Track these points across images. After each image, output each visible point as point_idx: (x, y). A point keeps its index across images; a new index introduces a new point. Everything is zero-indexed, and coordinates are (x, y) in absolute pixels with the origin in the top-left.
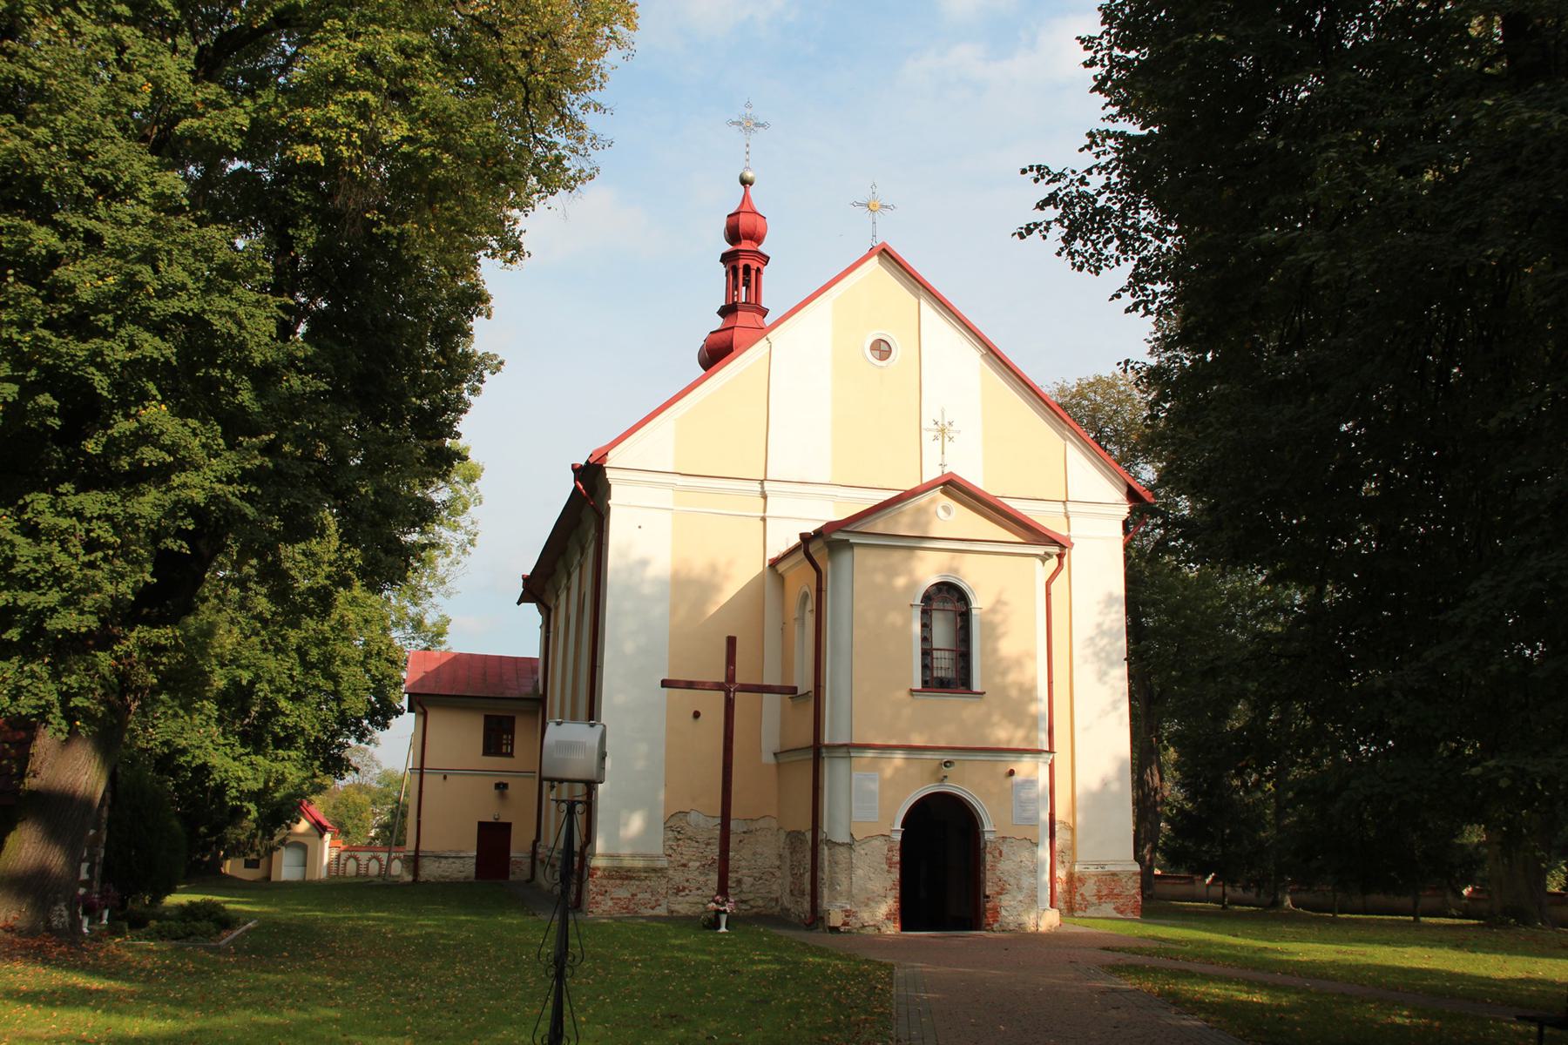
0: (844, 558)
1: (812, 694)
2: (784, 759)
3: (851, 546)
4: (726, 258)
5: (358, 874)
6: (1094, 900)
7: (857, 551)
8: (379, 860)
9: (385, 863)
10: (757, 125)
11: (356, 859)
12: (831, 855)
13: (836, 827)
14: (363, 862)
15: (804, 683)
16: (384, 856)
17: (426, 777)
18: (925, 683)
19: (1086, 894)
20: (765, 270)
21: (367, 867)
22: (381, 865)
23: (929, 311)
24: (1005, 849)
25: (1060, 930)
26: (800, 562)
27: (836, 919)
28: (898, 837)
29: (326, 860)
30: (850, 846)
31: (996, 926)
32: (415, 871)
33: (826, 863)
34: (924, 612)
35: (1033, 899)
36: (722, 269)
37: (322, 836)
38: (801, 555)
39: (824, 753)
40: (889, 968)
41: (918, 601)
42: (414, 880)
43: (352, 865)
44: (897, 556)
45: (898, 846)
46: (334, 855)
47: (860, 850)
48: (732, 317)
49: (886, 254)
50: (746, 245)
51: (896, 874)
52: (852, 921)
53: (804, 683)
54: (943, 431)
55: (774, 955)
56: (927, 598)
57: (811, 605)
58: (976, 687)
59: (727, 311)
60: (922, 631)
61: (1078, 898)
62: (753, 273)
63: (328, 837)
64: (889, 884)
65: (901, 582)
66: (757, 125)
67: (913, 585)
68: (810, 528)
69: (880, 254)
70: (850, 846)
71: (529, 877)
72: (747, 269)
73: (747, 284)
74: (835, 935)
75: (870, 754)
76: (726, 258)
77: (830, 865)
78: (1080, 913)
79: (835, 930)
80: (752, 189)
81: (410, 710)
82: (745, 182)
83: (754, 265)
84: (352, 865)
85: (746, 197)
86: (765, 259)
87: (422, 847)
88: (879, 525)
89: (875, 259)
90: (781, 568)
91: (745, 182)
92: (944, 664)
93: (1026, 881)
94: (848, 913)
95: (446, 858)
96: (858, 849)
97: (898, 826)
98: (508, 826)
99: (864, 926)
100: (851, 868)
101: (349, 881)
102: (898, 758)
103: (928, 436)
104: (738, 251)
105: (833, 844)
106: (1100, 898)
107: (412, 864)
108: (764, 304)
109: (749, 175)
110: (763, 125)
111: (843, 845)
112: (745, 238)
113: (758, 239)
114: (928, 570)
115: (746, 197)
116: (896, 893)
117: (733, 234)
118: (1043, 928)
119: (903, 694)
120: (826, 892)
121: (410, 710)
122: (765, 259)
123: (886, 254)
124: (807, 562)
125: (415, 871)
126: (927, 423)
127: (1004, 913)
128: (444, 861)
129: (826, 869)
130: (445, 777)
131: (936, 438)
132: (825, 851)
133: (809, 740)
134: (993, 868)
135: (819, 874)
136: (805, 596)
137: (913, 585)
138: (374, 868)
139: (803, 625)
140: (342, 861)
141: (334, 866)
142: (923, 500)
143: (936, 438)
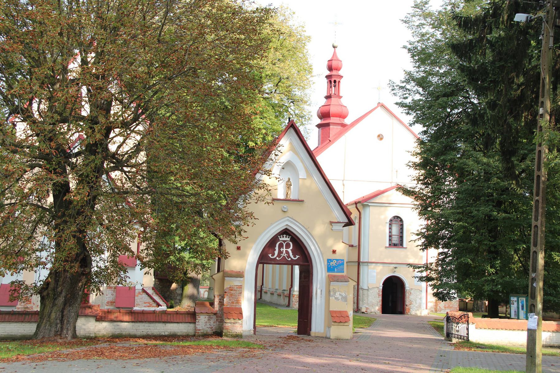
0: (367, 209)
2: (349, 264)
3: (369, 206)
4: (328, 77)
6: (443, 308)
7: (371, 207)
12: (362, 292)
13: (364, 284)
18: (390, 245)
19: (441, 306)
20: (342, 81)
24: (412, 292)
25: (428, 315)
27: (364, 310)
28: (381, 288)
31: (409, 313)
34: (390, 224)
35: (420, 306)
36: (326, 81)
38: (355, 205)
39: (361, 264)
41: (388, 221)
44: (382, 209)
45: (381, 290)
47: (371, 291)
48: (329, 100)
50: (334, 73)
51: (381, 298)
52: (368, 310)
55: (503, 89)
56: (391, 220)
58: (405, 246)
59: (328, 97)
61: (438, 307)
62: (337, 83)
64: (378, 301)
70: (368, 290)
71: (259, 298)
72: (335, 82)
73: (335, 86)
74: (364, 314)
75: (374, 265)
76: (328, 77)
78: (439, 312)
79: (363, 313)
80: (336, 49)
82: (334, 47)
85: (335, 52)
88: (377, 200)
92: (395, 240)
93: (418, 301)
94: (367, 308)
97: (381, 285)
98: (383, 313)
100: (368, 296)
105: (363, 289)
106: (445, 308)
108: (341, 95)
109: (335, 45)
112: (334, 70)
113: (338, 69)
114: (391, 213)
115: (335, 52)
117: (330, 68)
118: (423, 315)
119: (383, 249)
123: (383, 106)
127: (411, 310)
132: (361, 291)
133: (357, 260)
134: (409, 297)
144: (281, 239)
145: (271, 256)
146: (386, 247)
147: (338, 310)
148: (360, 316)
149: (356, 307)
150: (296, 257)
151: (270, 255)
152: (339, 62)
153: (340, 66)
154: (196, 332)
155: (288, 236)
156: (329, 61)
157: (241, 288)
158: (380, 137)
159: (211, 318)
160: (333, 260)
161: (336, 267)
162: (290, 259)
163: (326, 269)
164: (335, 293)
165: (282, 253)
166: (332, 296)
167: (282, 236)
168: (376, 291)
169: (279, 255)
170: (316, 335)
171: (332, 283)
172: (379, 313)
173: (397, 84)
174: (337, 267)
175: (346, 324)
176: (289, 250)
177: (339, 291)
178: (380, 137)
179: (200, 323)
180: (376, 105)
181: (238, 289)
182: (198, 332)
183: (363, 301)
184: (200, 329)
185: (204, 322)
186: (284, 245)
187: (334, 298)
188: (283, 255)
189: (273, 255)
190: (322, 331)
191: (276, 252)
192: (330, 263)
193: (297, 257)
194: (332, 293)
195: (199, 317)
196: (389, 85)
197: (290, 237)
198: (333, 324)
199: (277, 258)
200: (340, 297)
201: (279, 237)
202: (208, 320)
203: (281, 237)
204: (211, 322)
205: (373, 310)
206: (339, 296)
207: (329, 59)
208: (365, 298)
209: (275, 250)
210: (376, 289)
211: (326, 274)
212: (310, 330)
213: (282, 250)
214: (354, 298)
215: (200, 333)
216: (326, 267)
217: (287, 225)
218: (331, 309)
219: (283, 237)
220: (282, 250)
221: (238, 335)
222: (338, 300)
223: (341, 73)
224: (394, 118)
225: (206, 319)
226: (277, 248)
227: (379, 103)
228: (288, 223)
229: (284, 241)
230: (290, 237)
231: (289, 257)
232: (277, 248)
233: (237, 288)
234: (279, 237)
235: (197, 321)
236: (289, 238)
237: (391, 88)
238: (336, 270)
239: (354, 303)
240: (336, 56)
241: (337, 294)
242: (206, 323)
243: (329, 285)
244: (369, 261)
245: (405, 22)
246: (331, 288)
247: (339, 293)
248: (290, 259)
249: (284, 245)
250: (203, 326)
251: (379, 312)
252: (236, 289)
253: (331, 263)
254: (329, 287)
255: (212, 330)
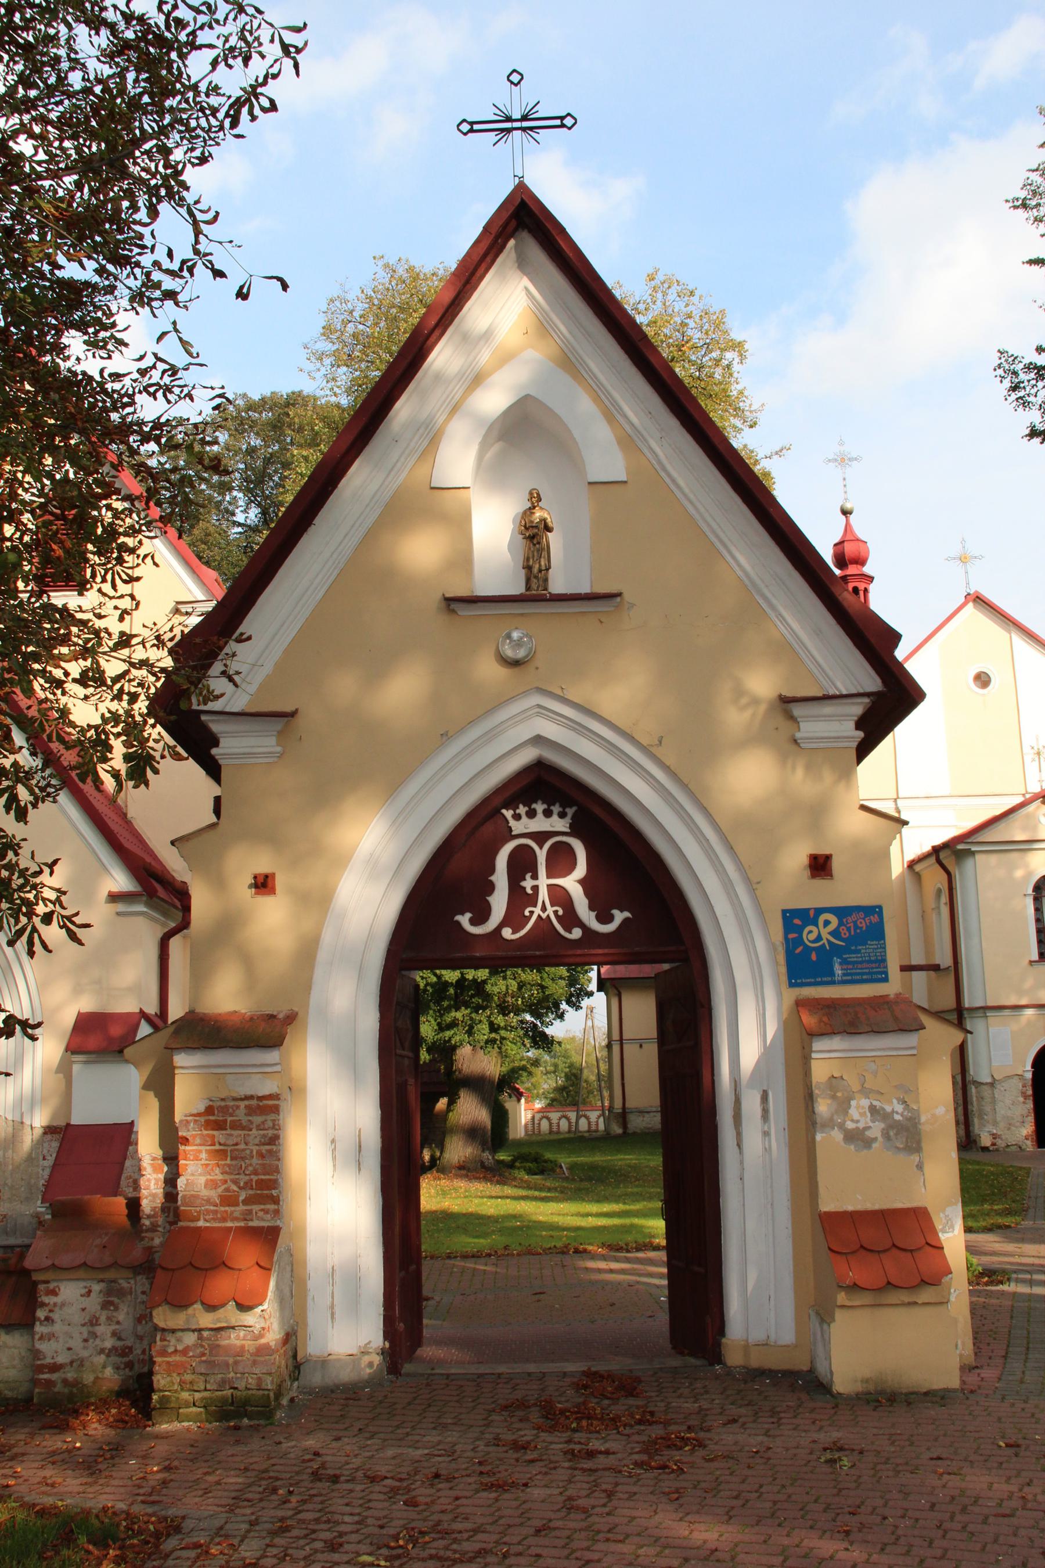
0: (969, 863)
1: (952, 968)
5: (551, 1132)
7: (978, 857)
8: (568, 1119)
9: (573, 1120)
10: (850, 459)
11: (548, 1119)
12: (978, 1092)
14: (555, 1121)
15: (945, 959)
16: (573, 1116)
17: (625, 1046)
20: (872, 588)
21: (558, 1125)
22: (570, 1123)
23: (1018, 641)
26: (932, 865)
27: (986, 1141)
28: (1029, 1076)
29: (523, 1122)
30: (992, 1085)
32: (624, 1125)
33: (974, 1099)
37: (519, 1100)
38: (933, 860)
39: (966, 1014)
40: (1028, 1171)
41: (1030, 891)
42: (624, 1133)
43: (545, 1124)
44: (1015, 855)
45: (1030, 1083)
46: (529, 1116)
49: (979, 600)
50: (852, 570)
51: (1030, 1105)
52: (999, 1142)
53: (945, 959)
54: (1039, 754)
57: (944, 899)
60: (1036, 914)
62: (861, 593)
63: (523, 1100)
64: (1025, 1112)
65: (1019, 873)
66: (850, 459)
67: (1030, 874)
68: (938, 841)
69: (974, 601)
70: (992, 1085)
77: (978, 1100)
79: (985, 1149)
80: (852, 517)
81: (599, 989)
82: (846, 513)
83: (861, 586)
84: (545, 1124)
85: (848, 528)
86: (871, 579)
87: (627, 1105)
89: (970, 605)
90: (918, 868)
91: (846, 513)
94: (995, 1136)
95: (648, 1112)
96: (998, 1086)
97: (1029, 1067)
99: (1008, 1146)
100: (994, 1101)
101: (562, 1137)
102: (1030, 1012)
103: (1028, 759)
104: (846, 576)
107: (621, 1120)
109: (848, 506)
110: (856, 459)
111: (987, 1084)
113: (861, 561)
115: (848, 528)
116: (1031, 1119)
120: (976, 1121)
121: (599, 989)
122: (871, 579)
123: (979, 600)
124: (937, 865)
125: (624, 1125)
126: (1027, 749)
128: (647, 1115)
129: (975, 1103)
130: (641, 1046)
131: (1034, 760)
132: (973, 1090)
135: (970, 1107)
136: (939, 891)
137: (1030, 874)
138: (564, 1125)
139: (939, 913)
140: (536, 1122)
141: (530, 1127)
142: (1031, 808)
143: (1034, 760)
144: (517, 827)
145: (473, 922)
146: (1031, 962)
147: (869, 1206)
148: (978, 1163)
149: (962, 1132)
150: (609, 919)
151: (464, 920)
152: (861, 544)
153: (862, 554)
154: (35, 1382)
155: (556, 809)
156: (835, 545)
157: (276, 1109)
158: (983, 680)
159: (121, 1293)
160: (819, 911)
161: (835, 950)
162: (576, 933)
163: (783, 969)
164: (844, 1106)
165: (532, 899)
166: (829, 1124)
167: (522, 810)
168: (1016, 1085)
169: (514, 917)
170: (755, 1363)
171: (818, 1045)
172: (1029, 1146)
173: (1026, 361)
174: (846, 950)
175: (926, 1295)
176: (572, 883)
177: (865, 1092)
178: (983, 680)
179: (58, 1328)
180: (963, 600)
181: (257, 1119)
182: (49, 1383)
183: (981, 1117)
184: (61, 1359)
185: (78, 1318)
186: (541, 855)
187: (837, 1135)
188: (537, 911)
189: (482, 915)
190: (787, 1336)
191: (499, 902)
192: (800, 930)
193: (619, 916)
194: (823, 1107)
195: (54, 1293)
196: (1000, 372)
197: (570, 811)
198: (841, 1298)
199: (507, 933)
200: (876, 1130)
201: (508, 814)
202: (106, 1305)
203: (517, 817)
204: (121, 1316)
205: (1012, 1141)
206: (865, 1121)
207: (837, 540)
208: (988, 1108)
209: (491, 888)
210: (1015, 1080)
211: (779, 995)
212: (721, 1328)
213: (528, 884)
214: (956, 1109)
215: (59, 1388)
216: (782, 958)
217: (538, 740)
218: (827, 1205)
219: (531, 814)
220: (528, 884)
221: (246, 1402)
222: (868, 1143)
223: (867, 569)
224: (1012, 628)
225: (93, 1303)
226: (501, 878)
227: (969, 594)
228: (551, 730)
229: (540, 837)
230: (570, 811)
231: (570, 918)
232: (501, 878)
233: (251, 1111)
234: (508, 814)
235: (41, 1314)
236: (562, 815)
237: (1007, 383)
238: (838, 971)
239: (957, 1123)
240: (852, 532)
241: (858, 1113)
242: (94, 1322)
243: (806, 1059)
244: (990, 1004)
245: (1024, 206)
246: (820, 1070)
247: (865, 1103)
248: (576, 933)
249: (541, 855)
250: (76, 1343)
251: (1029, 1143)
252: (244, 1119)
253: (810, 934)
254: (807, 1073)
255: (130, 1365)
